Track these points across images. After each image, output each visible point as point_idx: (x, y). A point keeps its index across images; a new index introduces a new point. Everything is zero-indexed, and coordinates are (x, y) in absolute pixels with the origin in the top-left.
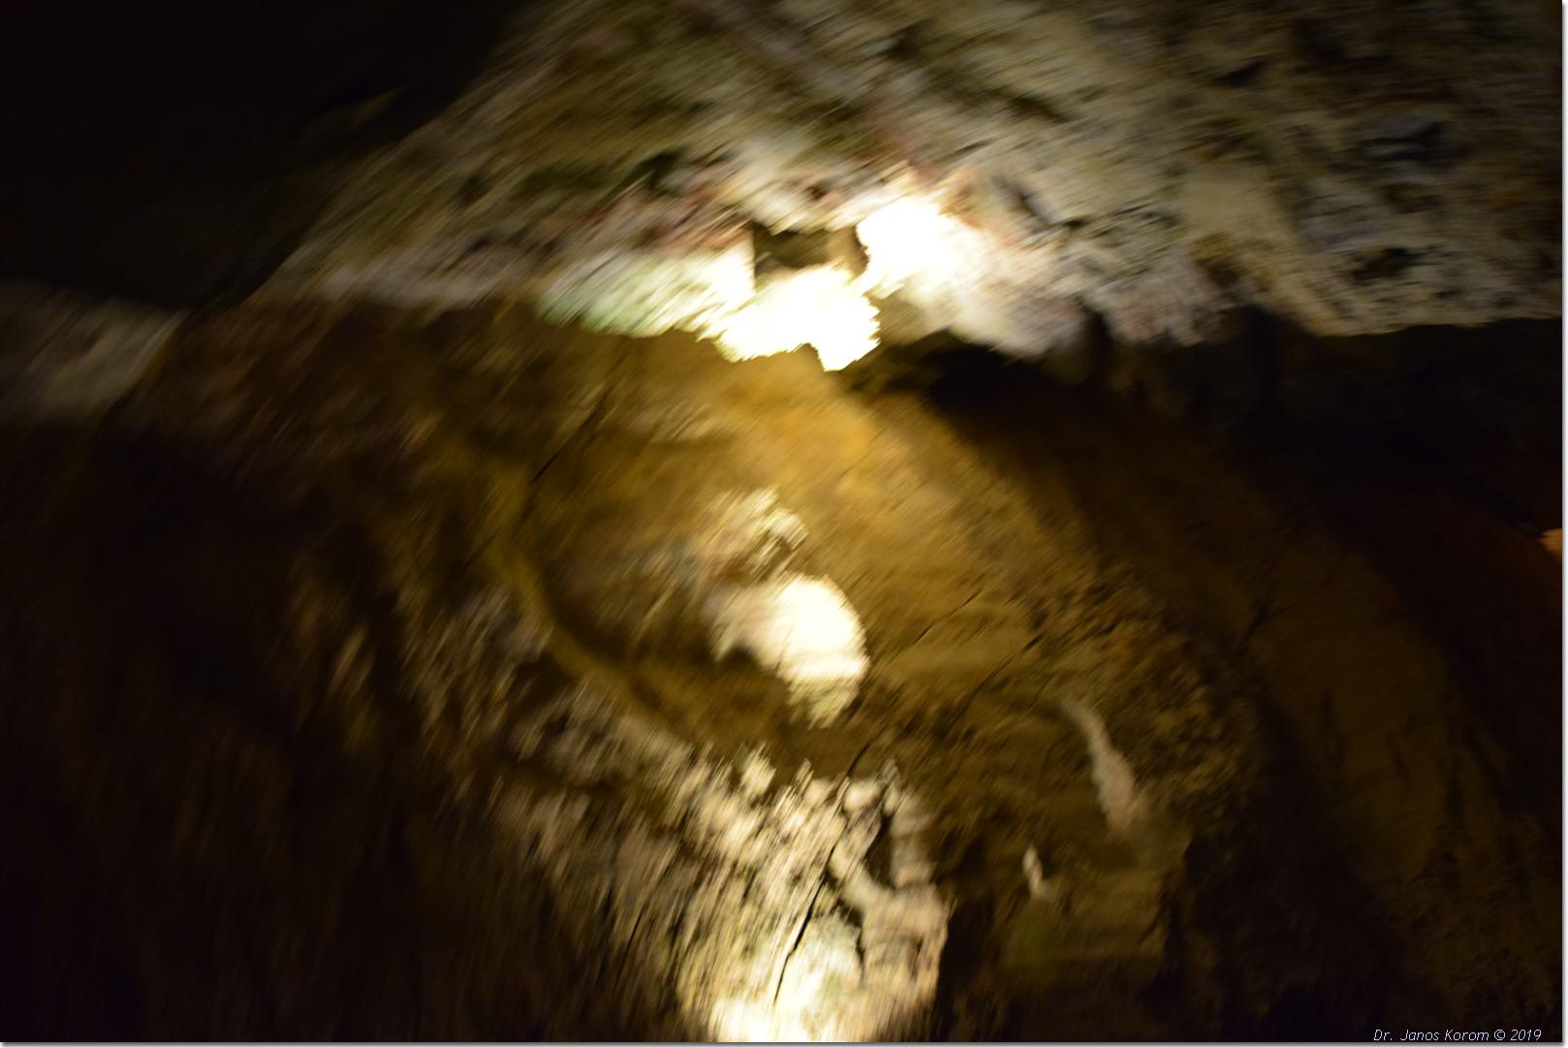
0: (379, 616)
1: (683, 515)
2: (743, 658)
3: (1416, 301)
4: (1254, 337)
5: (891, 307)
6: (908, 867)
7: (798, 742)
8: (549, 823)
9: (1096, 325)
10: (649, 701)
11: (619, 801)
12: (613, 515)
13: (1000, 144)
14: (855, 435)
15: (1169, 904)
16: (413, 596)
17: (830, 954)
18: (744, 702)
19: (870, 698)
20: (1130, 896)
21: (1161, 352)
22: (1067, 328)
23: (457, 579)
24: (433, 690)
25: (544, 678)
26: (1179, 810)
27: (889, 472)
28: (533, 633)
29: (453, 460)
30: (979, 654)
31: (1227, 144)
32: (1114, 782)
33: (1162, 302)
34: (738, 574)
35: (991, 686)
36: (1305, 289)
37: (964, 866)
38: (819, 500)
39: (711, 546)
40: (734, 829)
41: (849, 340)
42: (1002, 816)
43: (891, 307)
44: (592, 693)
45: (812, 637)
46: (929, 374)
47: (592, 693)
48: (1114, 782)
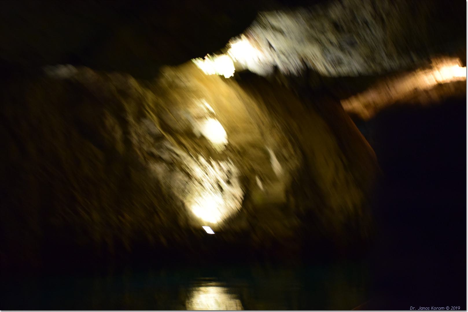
0: (124, 123)
1: (186, 102)
2: (203, 137)
3: (344, 70)
4: (308, 72)
5: (236, 64)
6: (235, 181)
7: (211, 154)
8: (159, 170)
9: (276, 68)
10: (181, 145)
11: (174, 165)
12: (171, 103)
13: (270, 37)
14: (224, 88)
15: (287, 192)
16: (131, 119)
17: (218, 197)
18: (200, 145)
19: (229, 147)
20: (278, 190)
21: (290, 76)
22: (270, 70)
23: (141, 115)
24: (135, 139)
25: (159, 138)
26: (291, 173)
27: (234, 100)
28: (157, 129)
29: (140, 90)
30: (249, 138)
31: (315, 40)
32: (276, 166)
33: (289, 64)
34: (200, 118)
35: (253, 145)
36: (322, 65)
37: (246, 182)
38: (218, 105)
39: (193, 111)
40: (197, 171)
41: (229, 73)
42: (253, 171)
43: (236, 64)
44: (170, 143)
45: (215, 133)
46: (244, 78)
47: (170, 143)
48: (276, 166)
